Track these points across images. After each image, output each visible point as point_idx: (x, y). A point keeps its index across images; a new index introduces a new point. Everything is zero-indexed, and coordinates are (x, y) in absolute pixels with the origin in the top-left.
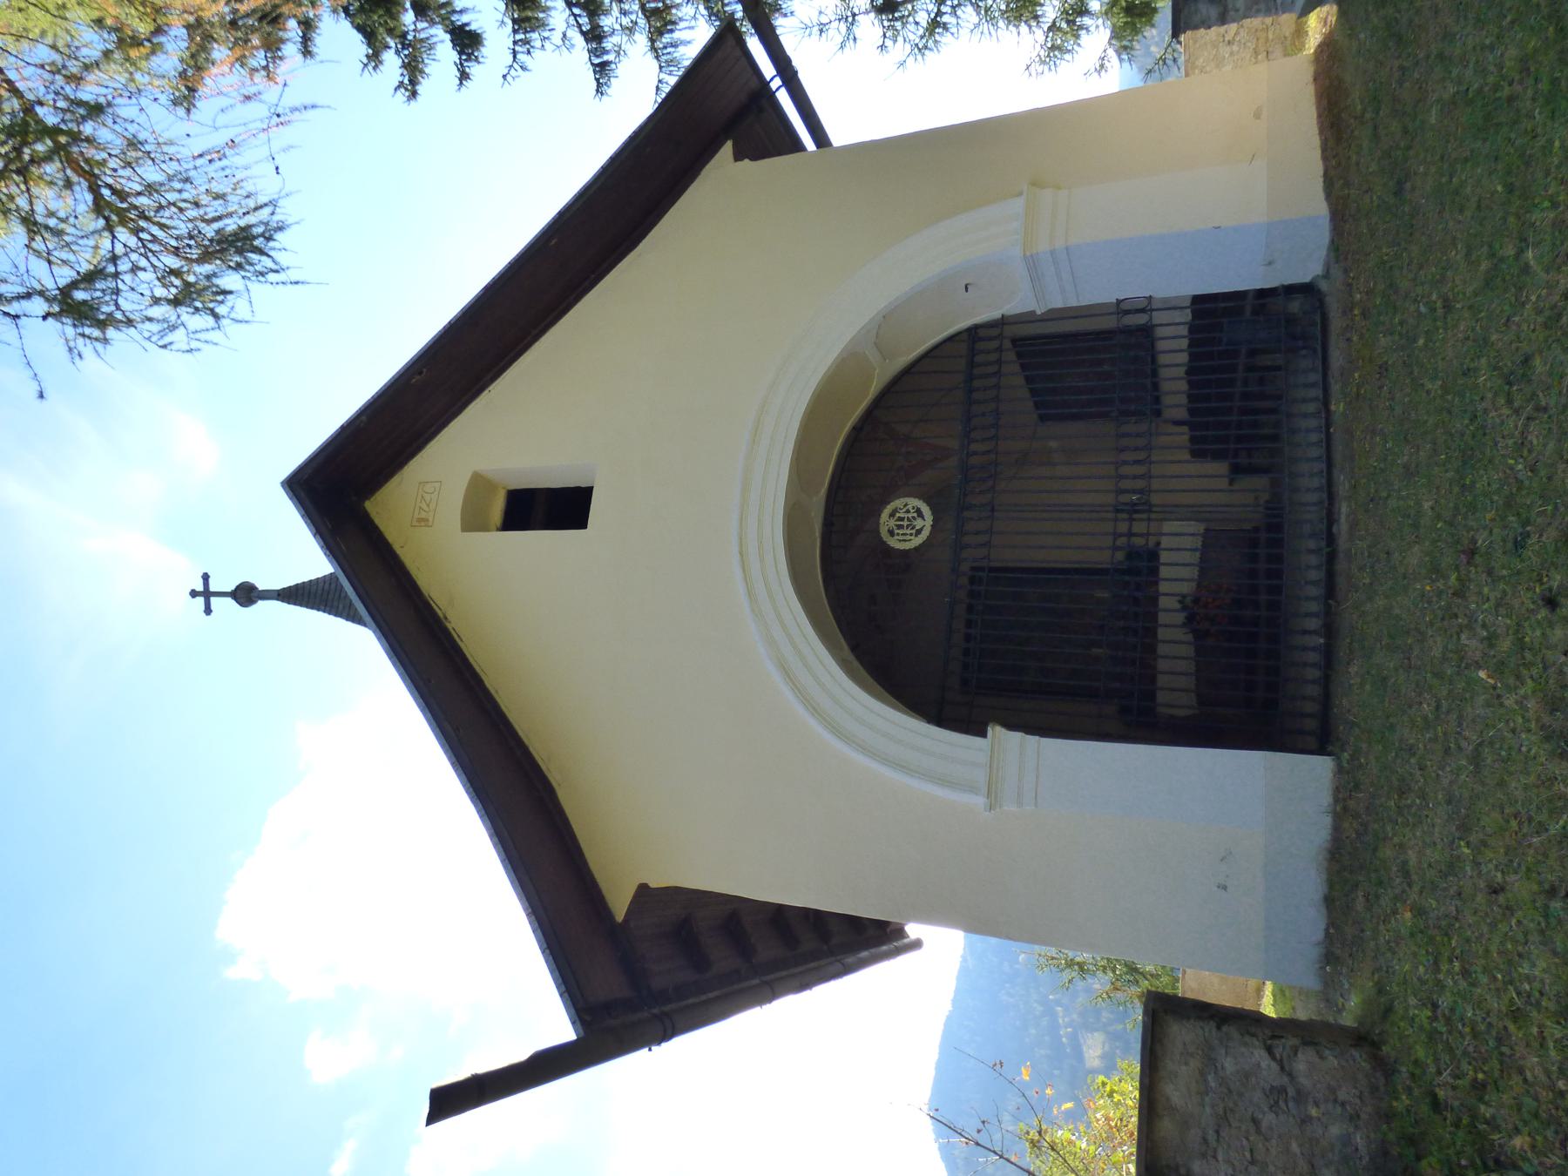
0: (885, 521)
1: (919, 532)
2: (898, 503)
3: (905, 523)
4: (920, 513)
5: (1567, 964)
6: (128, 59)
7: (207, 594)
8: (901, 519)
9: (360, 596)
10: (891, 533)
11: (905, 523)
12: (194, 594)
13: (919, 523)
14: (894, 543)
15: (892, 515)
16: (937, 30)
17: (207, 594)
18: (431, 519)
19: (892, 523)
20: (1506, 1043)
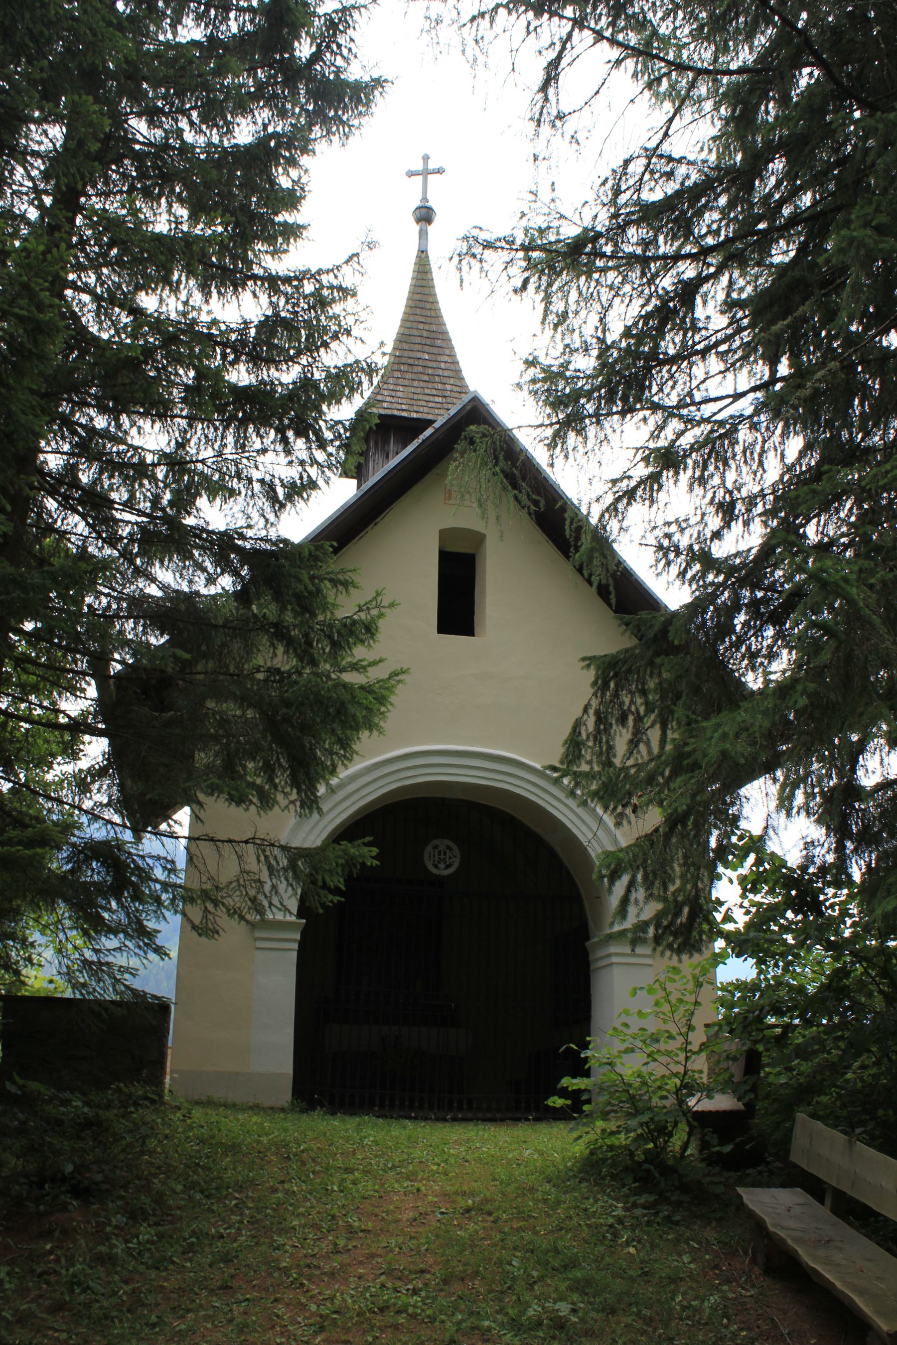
0: (443, 843)
1: (436, 866)
2: (456, 851)
3: (442, 857)
4: (448, 867)
5: (6, 863)
6: (554, 1166)
7: (425, 173)
8: (445, 854)
9: (424, 441)
10: (436, 847)
11: (442, 857)
12: (426, 158)
13: (442, 866)
14: (429, 849)
15: (448, 848)
16: (18, 212)
17: (425, 173)
18: (451, 502)
19: (442, 848)
20: (90, 702)
